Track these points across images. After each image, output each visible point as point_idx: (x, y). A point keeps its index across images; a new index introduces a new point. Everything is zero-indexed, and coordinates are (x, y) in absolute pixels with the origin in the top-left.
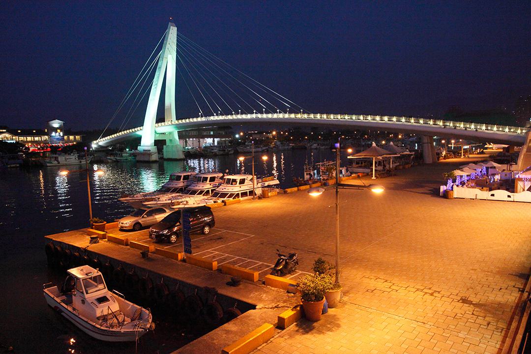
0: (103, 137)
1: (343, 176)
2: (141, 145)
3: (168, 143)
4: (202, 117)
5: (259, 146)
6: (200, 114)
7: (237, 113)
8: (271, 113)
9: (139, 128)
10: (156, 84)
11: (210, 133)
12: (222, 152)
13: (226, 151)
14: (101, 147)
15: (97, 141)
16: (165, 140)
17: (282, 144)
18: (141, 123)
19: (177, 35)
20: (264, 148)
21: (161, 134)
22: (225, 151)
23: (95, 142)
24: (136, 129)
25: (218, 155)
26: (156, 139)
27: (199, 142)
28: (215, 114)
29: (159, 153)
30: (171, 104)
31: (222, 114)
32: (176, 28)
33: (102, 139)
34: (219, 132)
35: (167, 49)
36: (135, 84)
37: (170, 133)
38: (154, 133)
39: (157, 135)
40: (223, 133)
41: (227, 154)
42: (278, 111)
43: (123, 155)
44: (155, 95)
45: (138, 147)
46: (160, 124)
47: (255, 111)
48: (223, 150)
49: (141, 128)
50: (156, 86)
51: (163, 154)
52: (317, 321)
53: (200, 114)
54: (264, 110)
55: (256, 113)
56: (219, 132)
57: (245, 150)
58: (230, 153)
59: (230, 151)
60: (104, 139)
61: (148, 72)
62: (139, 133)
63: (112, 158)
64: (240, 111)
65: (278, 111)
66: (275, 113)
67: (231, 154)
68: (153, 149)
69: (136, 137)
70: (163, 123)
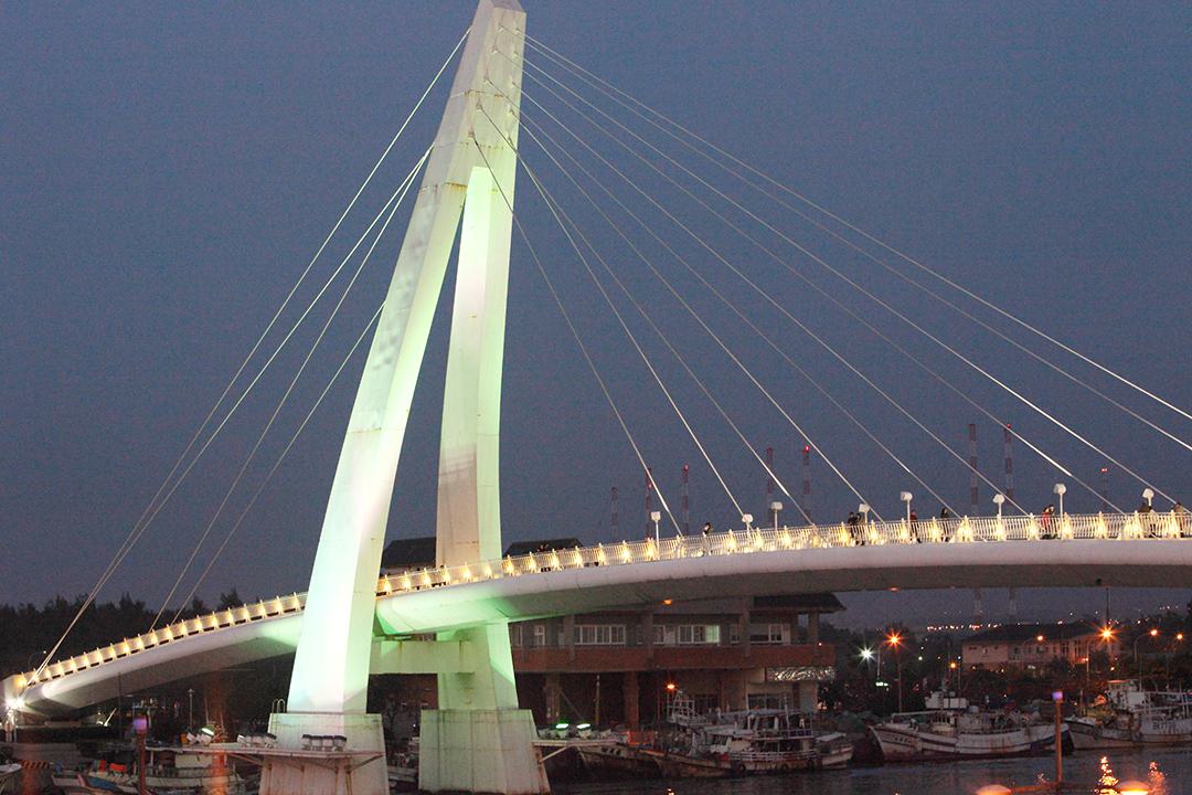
0: (62, 656)
1: (407, 756)
2: (290, 707)
3: (447, 696)
4: (668, 533)
5: (1014, 716)
6: (656, 516)
7: (889, 512)
8: (1107, 510)
9: (278, 605)
10: (393, 341)
11: (701, 635)
12: (775, 758)
13: (806, 749)
14: (48, 709)
15: (35, 676)
16: (433, 677)
17: (1156, 701)
18: (294, 576)
19: (528, 53)
20: (1044, 732)
21: (414, 637)
22: (797, 745)
23: (21, 681)
24: (262, 610)
25: (752, 773)
26: (382, 671)
27: (448, 705)
28: (748, 518)
29: (391, 761)
30: (475, 446)
31: (793, 520)
32: (525, 15)
33: (59, 668)
34: (758, 630)
35: (464, 136)
36: (285, 324)
37: (465, 635)
38: (370, 634)
39: (388, 647)
40: (786, 638)
41: (814, 769)
42: (1148, 494)
43: (180, 762)
44: (381, 407)
45: (273, 717)
46: (406, 580)
47: (999, 499)
48: (784, 745)
49: (295, 602)
50: (389, 352)
51: (414, 764)
52: (31, 607)
53: (656, 516)
54: (1062, 489)
55: (1008, 510)
56: (758, 630)
57: (923, 741)
58: (826, 761)
59: (826, 750)
60: (72, 664)
61: (351, 267)
62: (279, 631)
63: (117, 778)
64: (908, 496)
65: (1148, 494)
66: (1129, 511)
67: (834, 767)
68: (366, 734)
69: (271, 653)
70: (425, 577)
